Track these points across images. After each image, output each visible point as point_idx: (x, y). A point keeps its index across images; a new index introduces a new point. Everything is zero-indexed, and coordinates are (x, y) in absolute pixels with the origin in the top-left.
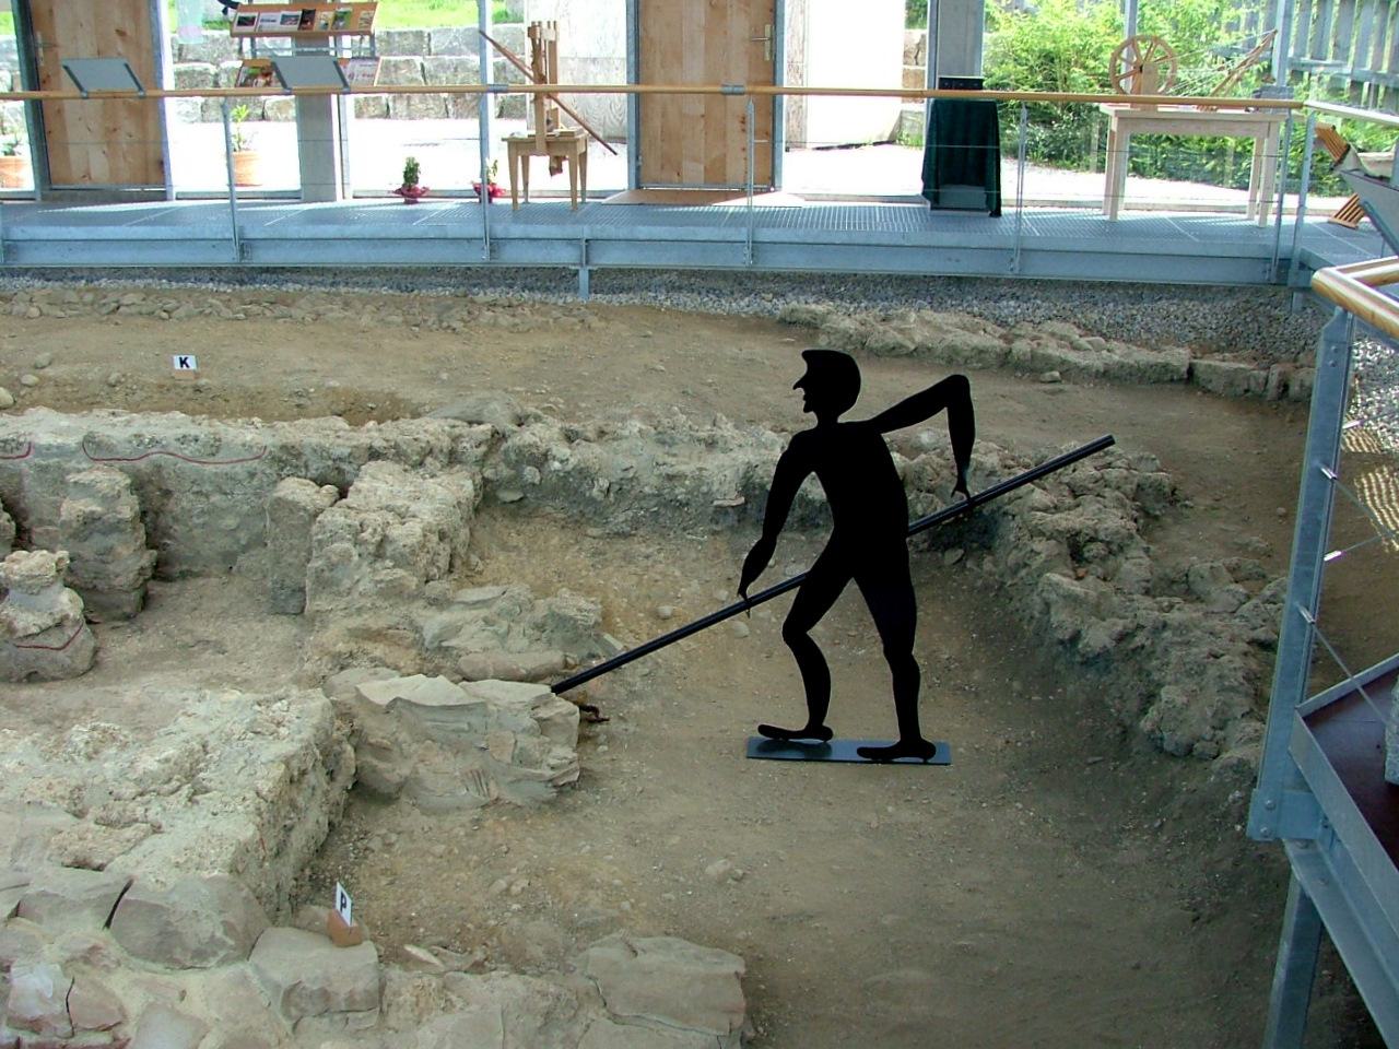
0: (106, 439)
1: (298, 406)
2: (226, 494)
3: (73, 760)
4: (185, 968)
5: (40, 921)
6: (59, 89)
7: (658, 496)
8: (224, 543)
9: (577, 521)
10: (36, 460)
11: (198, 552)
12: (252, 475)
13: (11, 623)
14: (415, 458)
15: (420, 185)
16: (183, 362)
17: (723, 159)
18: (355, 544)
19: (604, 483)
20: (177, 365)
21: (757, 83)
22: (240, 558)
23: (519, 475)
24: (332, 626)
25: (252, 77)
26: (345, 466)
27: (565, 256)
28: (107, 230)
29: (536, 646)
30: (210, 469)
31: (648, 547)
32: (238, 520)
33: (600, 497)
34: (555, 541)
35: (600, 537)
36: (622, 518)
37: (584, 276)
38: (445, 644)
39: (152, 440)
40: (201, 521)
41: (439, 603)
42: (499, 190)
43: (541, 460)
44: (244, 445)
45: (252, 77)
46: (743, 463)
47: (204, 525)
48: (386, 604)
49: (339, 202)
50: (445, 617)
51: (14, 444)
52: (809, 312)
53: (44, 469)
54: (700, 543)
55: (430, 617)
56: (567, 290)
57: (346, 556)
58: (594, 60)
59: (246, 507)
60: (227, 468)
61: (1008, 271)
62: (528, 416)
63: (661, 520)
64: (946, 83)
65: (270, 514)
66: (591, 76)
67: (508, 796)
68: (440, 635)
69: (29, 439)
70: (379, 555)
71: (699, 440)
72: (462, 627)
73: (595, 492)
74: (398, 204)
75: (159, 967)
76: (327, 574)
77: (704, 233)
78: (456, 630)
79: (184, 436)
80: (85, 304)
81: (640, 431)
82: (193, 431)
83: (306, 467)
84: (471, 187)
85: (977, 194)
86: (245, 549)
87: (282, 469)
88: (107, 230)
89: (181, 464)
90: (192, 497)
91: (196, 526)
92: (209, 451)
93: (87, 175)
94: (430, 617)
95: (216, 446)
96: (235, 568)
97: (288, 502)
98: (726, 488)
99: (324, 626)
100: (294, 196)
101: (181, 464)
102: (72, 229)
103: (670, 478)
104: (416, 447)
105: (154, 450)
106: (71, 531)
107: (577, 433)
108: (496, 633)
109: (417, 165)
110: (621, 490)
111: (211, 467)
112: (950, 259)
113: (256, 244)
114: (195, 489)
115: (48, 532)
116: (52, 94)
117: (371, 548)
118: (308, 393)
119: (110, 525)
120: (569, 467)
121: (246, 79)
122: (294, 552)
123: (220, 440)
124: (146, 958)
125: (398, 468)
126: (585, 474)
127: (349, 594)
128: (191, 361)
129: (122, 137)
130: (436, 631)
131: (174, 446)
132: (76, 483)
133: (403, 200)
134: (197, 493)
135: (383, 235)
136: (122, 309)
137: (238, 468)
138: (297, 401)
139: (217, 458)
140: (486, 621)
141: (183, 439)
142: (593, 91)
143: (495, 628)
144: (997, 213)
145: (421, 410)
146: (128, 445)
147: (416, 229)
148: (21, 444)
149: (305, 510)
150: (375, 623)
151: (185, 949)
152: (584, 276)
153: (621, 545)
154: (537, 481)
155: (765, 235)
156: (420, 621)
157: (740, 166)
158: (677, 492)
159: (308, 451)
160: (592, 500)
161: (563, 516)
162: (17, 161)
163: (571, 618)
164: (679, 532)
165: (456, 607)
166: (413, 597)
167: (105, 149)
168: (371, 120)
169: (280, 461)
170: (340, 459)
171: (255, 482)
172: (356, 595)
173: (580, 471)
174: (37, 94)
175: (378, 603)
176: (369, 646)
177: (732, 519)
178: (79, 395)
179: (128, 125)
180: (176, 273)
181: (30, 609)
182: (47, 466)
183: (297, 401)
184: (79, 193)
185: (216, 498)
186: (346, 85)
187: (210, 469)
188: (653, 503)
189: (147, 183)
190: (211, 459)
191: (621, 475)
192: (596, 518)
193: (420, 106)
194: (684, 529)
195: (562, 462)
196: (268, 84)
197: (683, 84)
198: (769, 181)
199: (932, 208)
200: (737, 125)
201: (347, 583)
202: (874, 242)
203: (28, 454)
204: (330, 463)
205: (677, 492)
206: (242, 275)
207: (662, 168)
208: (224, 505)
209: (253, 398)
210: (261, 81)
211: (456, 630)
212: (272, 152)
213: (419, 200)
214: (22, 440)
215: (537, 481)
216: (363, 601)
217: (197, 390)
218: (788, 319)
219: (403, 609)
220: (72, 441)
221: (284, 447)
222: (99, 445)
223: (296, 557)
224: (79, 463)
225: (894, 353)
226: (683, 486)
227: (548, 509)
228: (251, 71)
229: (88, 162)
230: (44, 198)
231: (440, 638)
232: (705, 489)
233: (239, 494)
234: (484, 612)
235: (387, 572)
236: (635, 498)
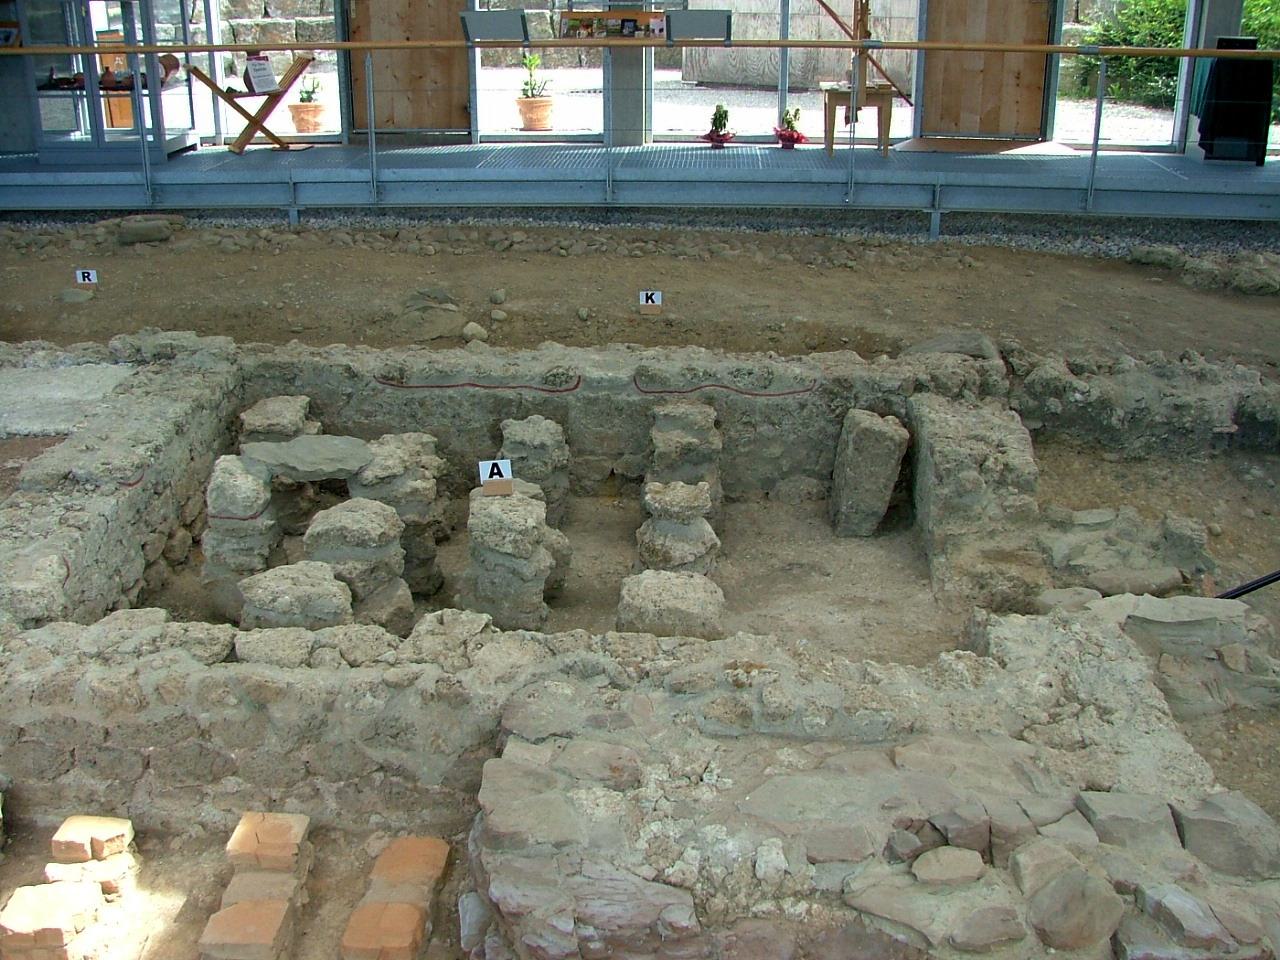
0: (659, 373)
1: (772, 339)
2: (773, 424)
3: (963, 687)
4: (1264, 879)
5: (1123, 844)
6: (368, 39)
7: (1167, 424)
8: (765, 470)
9: (1092, 447)
10: (586, 393)
11: (739, 479)
12: (803, 406)
13: (667, 552)
14: (956, 390)
15: (892, 135)
16: (648, 298)
17: (997, 110)
18: (980, 473)
19: (1120, 412)
20: (643, 301)
21: (1032, 42)
22: (778, 484)
23: (1042, 405)
24: (965, 548)
25: (574, 28)
26: (893, 398)
27: (917, 201)
28: (420, 173)
29: (1154, 563)
30: (761, 400)
31: (1161, 470)
32: (782, 449)
33: (1119, 426)
34: (1076, 465)
35: (1118, 462)
36: (1137, 444)
37: (936, 218)
38: (1072, 563)
39: (705, 373)
40: (747, 449)
41: (1064, 525)
42: (803, 137)
43: (1059, 392)
44: (796, 378)
45: (574, 28)
46: (1236, 394)
47: (747, 454)
48: (1013, 528)
49: (648, 145)
50: (1073, 538)
51: (563, 378)
52: (1164, 253)
53: (593, 402)
54: (1204, 466)
55: (1057, 539)
56: (919, 229)
57: (976, 483)
58: (755, 15)
59: (792, 437)
60: (779, 400)
61: (1074, 209)
62: (1012, 351)
63: (1170, 446)
64: (1224, 44)
65: (855, 443)
66: (751, 31)
67: (1245, 703)
68: (1069, 555)
69: (578, 373)
70: (1001, 483)
71: (1192, 374)
72: (1085, 548)
73: (1114, 421)
74: (706, 148)
75: (1241, 880)
76: (956, 500)
77: (993, 179)
78: (1080, 550)
79: (738, 370)
80: (472, 242)
81: (1136, 365)
82: (748, 365)
83: (856, 398)
84: (773, 133)
85: (1242, 144)
86: (784, 476)
87: (832, 401)
88: (420, 173)
89: (733, 396)
90: (740, 427)
91: (741, 454)
92: (762, 384)
93: (390, 120)
94: (1057, 539)
95: (768, 379)
96: (771, 494)
97: (874, 432)
98: (1224, 416)
99: (957, 547)
100: (597, 139)
101: (733, 396)
102: (445, 170)
103: (1177, 407)
104: (957, 380)
105: (707, 383)
106: (670, 461)
107: (1082, 367)
108: (1118, 552)
109: (726, 112)
110: (1136, 418)
111: (763, 398)
112: (1261, 206)
113: (388, 185)
114: (745, 420)
115: (587, 462)
116: (357, 44)
117: (996, 476)
118: (780, 327)
119: (704, 455)
120: (1093, 398)
121: (569, 30)
122: (873, 479)
123: (772, 373)
124: (1227, 872)
125: (942, 399)
126: (1105, 404)
127: (979, 519)
128: (658, 297)
129: (427, 83)
130: (1067, 552)
131: (727, 380)
132: (665, 415)
133: (710, 145)
134: (745, 423)
135: (750, 178)
136: (516, 246)
137: (790, 399)
138: (769, 334)
139: (772, 390)
140: (1109, 541)
141: (737, 373)
142: (754, 46)
143: (1118, 547)
144: (1261, 162)
145: (902, 344)
146: (682, 379)
147: (723, 173)
148: (571, 377)
149: (892, 439)
150: (1008, 544)
151: (1261, 862)
152: (936, 218)
153: (1138, 468)
154: (1059, 410)
155: (622, 174)
156: (1048, 543)
157: (1009, 121)
158: (1185, 420)
159: (859, 385)
160: (1110, 428)
161: (1079, 442)
162: (316, 107)
163: (1189, 537)
164: (1185, 456)
165: (1076, 529)
166: (1038, 521)
167: (410, 94)
168: (508, 70)
169: (831, 393)
170: (890, 391)
171: (805, 412)
172: (987, 520)
173: (1102, 402)
174: (348, 45)
175: (1008, 527)
176: (1003, 566)
177: (1224, 445)
178: (549, 329)
179: (434, 74)
180: (562, 212)
181: (684, 539)
182: (597, 399)
183: (769, 334)
184: (386, 136)
185: (764, 429)
186: (526, 37)
187: (761, 400)
188: (1163, 431)
189: (449, 127)
190: (763, 392)
191: (1135, 405)
192: (1113, 445)
193: (555, 56)
194: (1189, 454)
195: (1083, 393)
196: (591, 35)
197: (974, 42)
198: (1042, 132)
199: (1206, 158)
200: (1012, 81)
201: (978, 509)
202: (992, 184)
203: (576, 387)
204: (880, 395)
205: (1185, 420)
206: (605, 213)
207: (942, 118)
208: (771, 435)
209: (723, 331)
210: (584, 32)
211: (1080, 550)
212: (574, 99)
213: (725, 145)
214: (571, 373)
215: (1059, 410)
216: (993, 526)
217: (669, 323)
218: (1144, 260)
219: (1030, 532)
220: (625, 374)
221: (837, 381)
222: (652, 378)
223: (875, 483)
224: (628, 395)
225: (1261, 292)
226: (1190, 415)
227: (1064, 436)
228: (572, 23)
229: (393, 108)
230: (350, 141)
231: (1069, 558)
232: (1206, 417)
233: (787, 424)
234: (1102, 533)
235: (1015, 499)
236: (1147, 427)
